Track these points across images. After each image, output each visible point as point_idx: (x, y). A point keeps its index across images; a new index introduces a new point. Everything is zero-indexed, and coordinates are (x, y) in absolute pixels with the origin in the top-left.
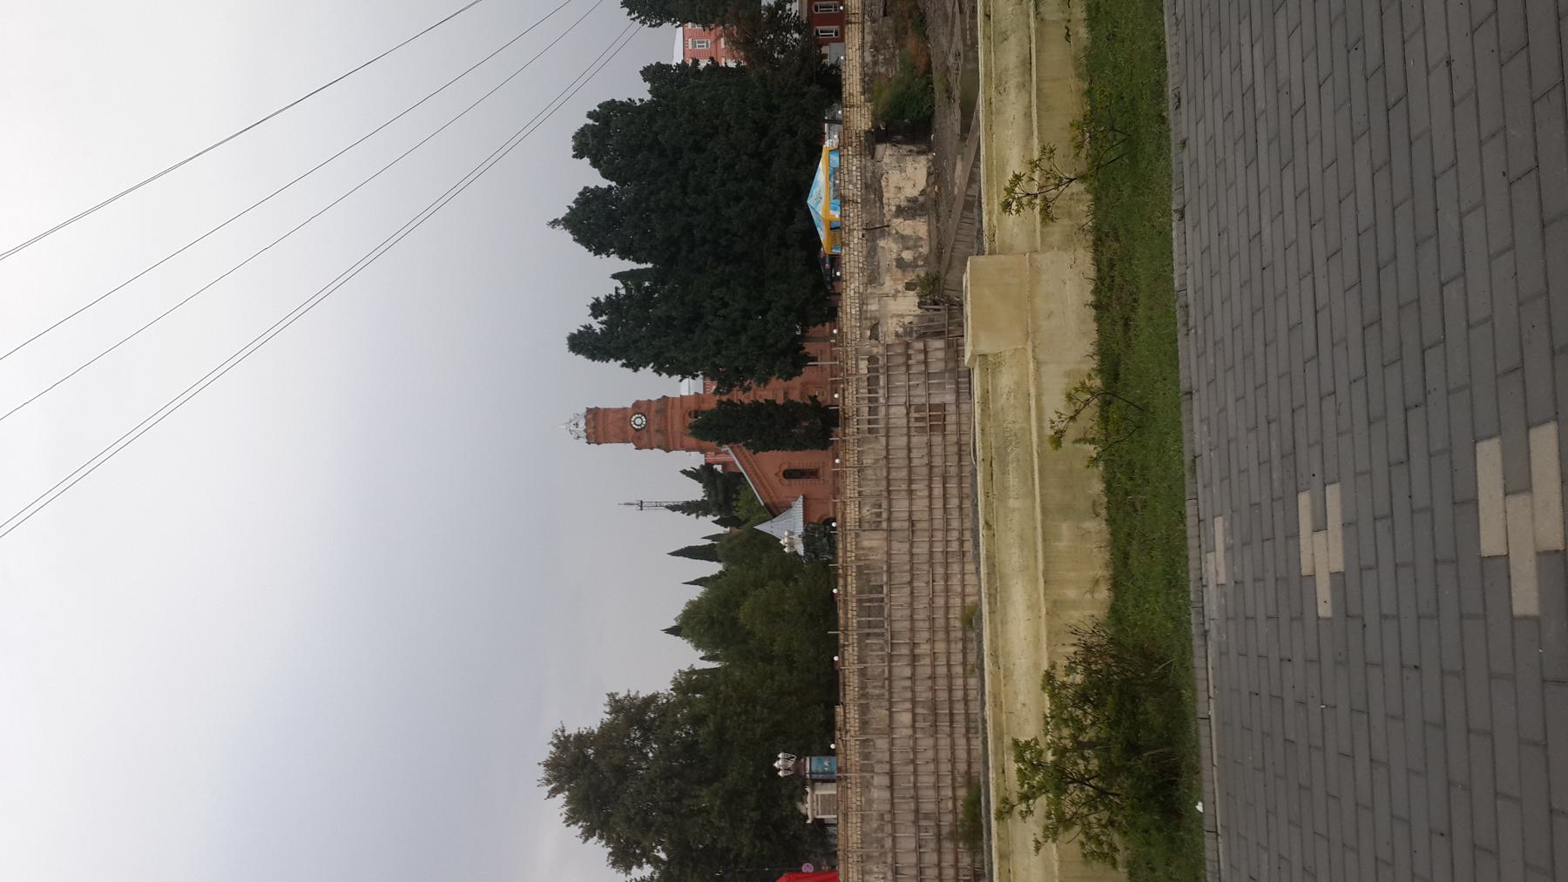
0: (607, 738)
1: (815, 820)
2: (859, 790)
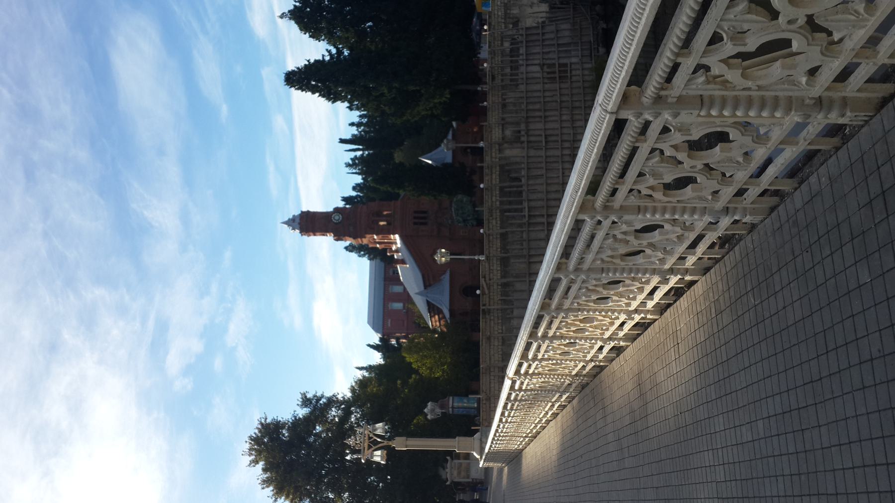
0: (300, 426)
1: (453, 482)
2: (500, 321)
